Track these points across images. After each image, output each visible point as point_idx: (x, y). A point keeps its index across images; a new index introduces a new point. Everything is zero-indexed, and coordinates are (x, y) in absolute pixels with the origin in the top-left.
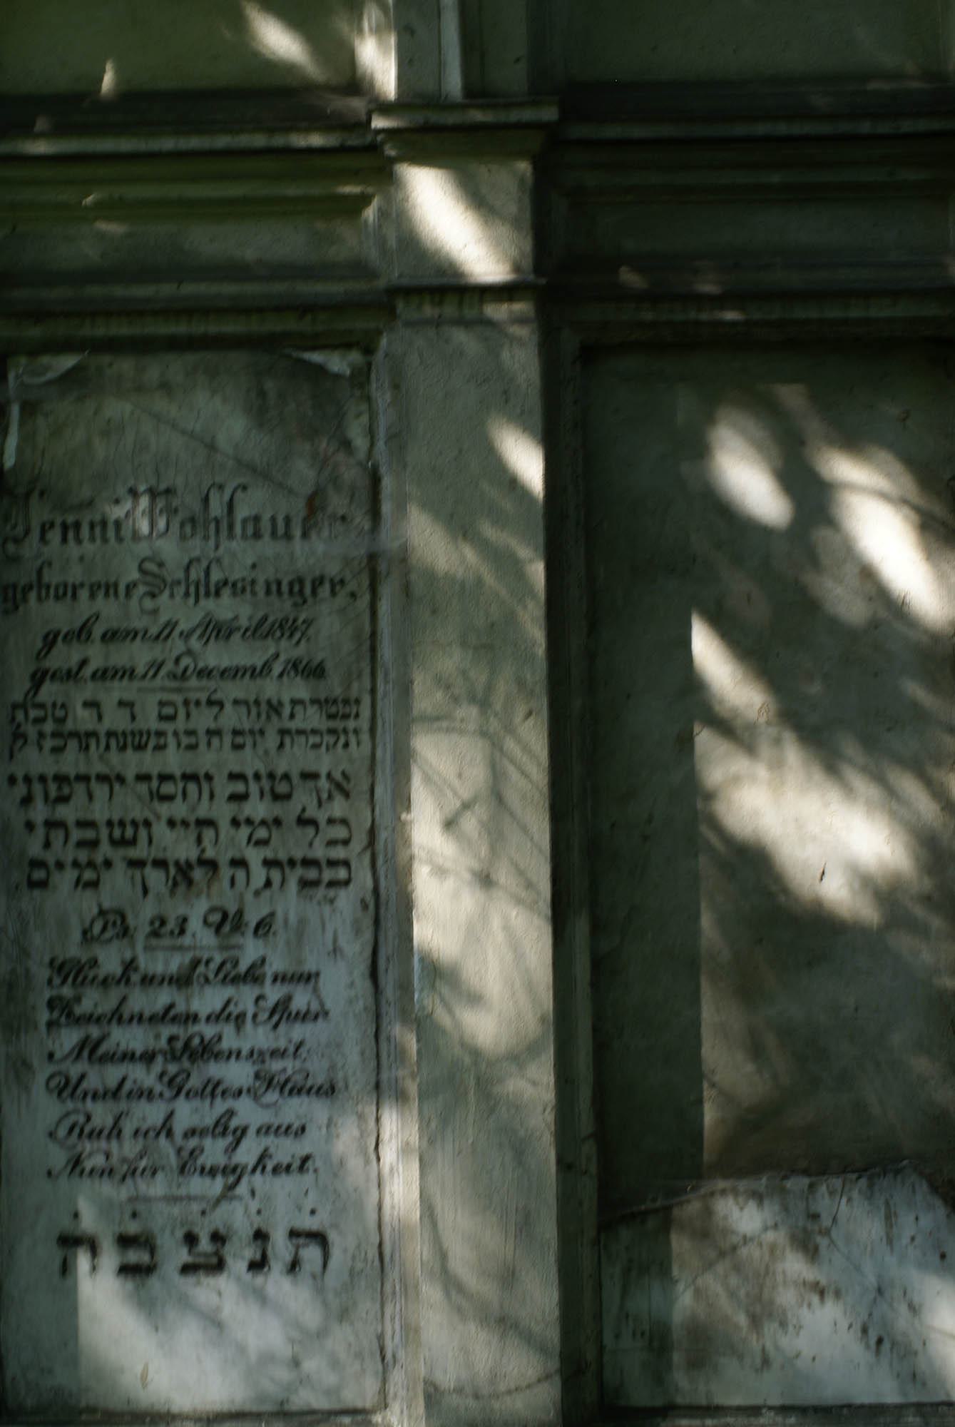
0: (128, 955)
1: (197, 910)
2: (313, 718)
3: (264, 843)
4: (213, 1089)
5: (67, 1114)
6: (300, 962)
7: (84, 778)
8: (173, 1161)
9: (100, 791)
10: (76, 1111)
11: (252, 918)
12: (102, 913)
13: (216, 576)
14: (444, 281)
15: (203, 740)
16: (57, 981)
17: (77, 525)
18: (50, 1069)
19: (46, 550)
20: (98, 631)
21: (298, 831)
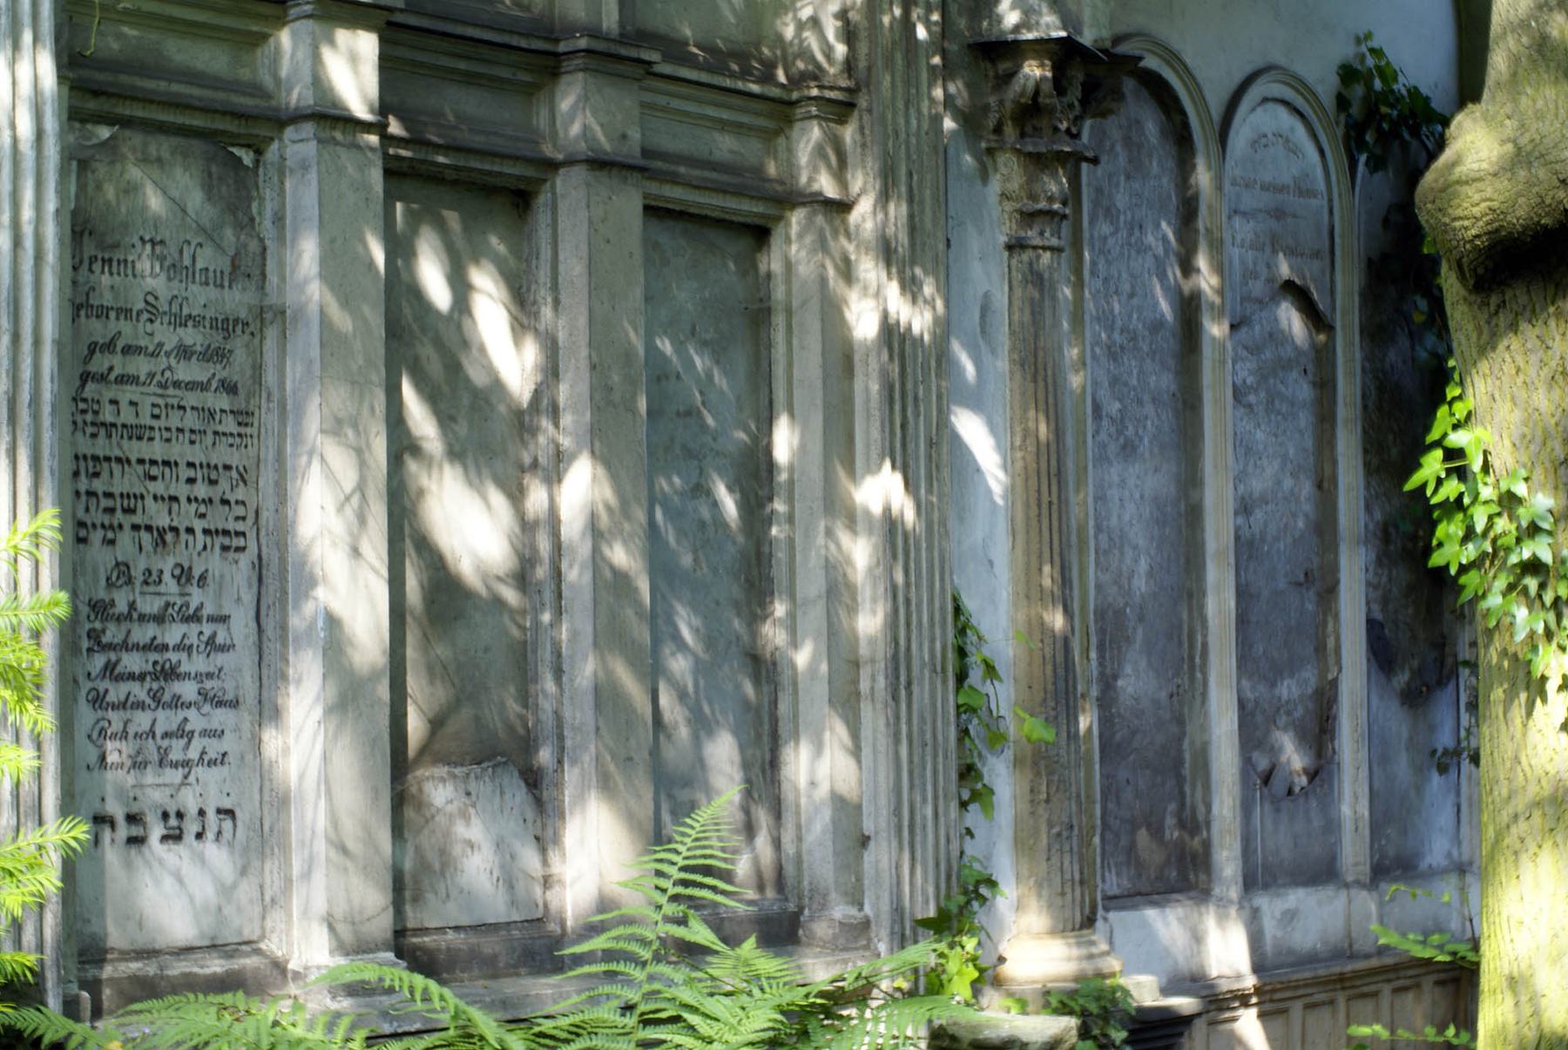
0: (131, 598)
1: (167, 564)
2: (229, 425)
3: (203, 516)
4: (177, 703)
5: (98, 721)
6: (220, 606)
7: (108, 459)
8: (155, 757)
9: (116, 468)
10: (103, 719)
11: (196, 573)
12: (117, 564)
13: (185, 311)
14: (337, 112)
15: (174, 433)
16: (92, 617)
17: (110, 260)
18: (90, 685)
19: (92, 277)
20: (120, 345)
21: (220, 507)
